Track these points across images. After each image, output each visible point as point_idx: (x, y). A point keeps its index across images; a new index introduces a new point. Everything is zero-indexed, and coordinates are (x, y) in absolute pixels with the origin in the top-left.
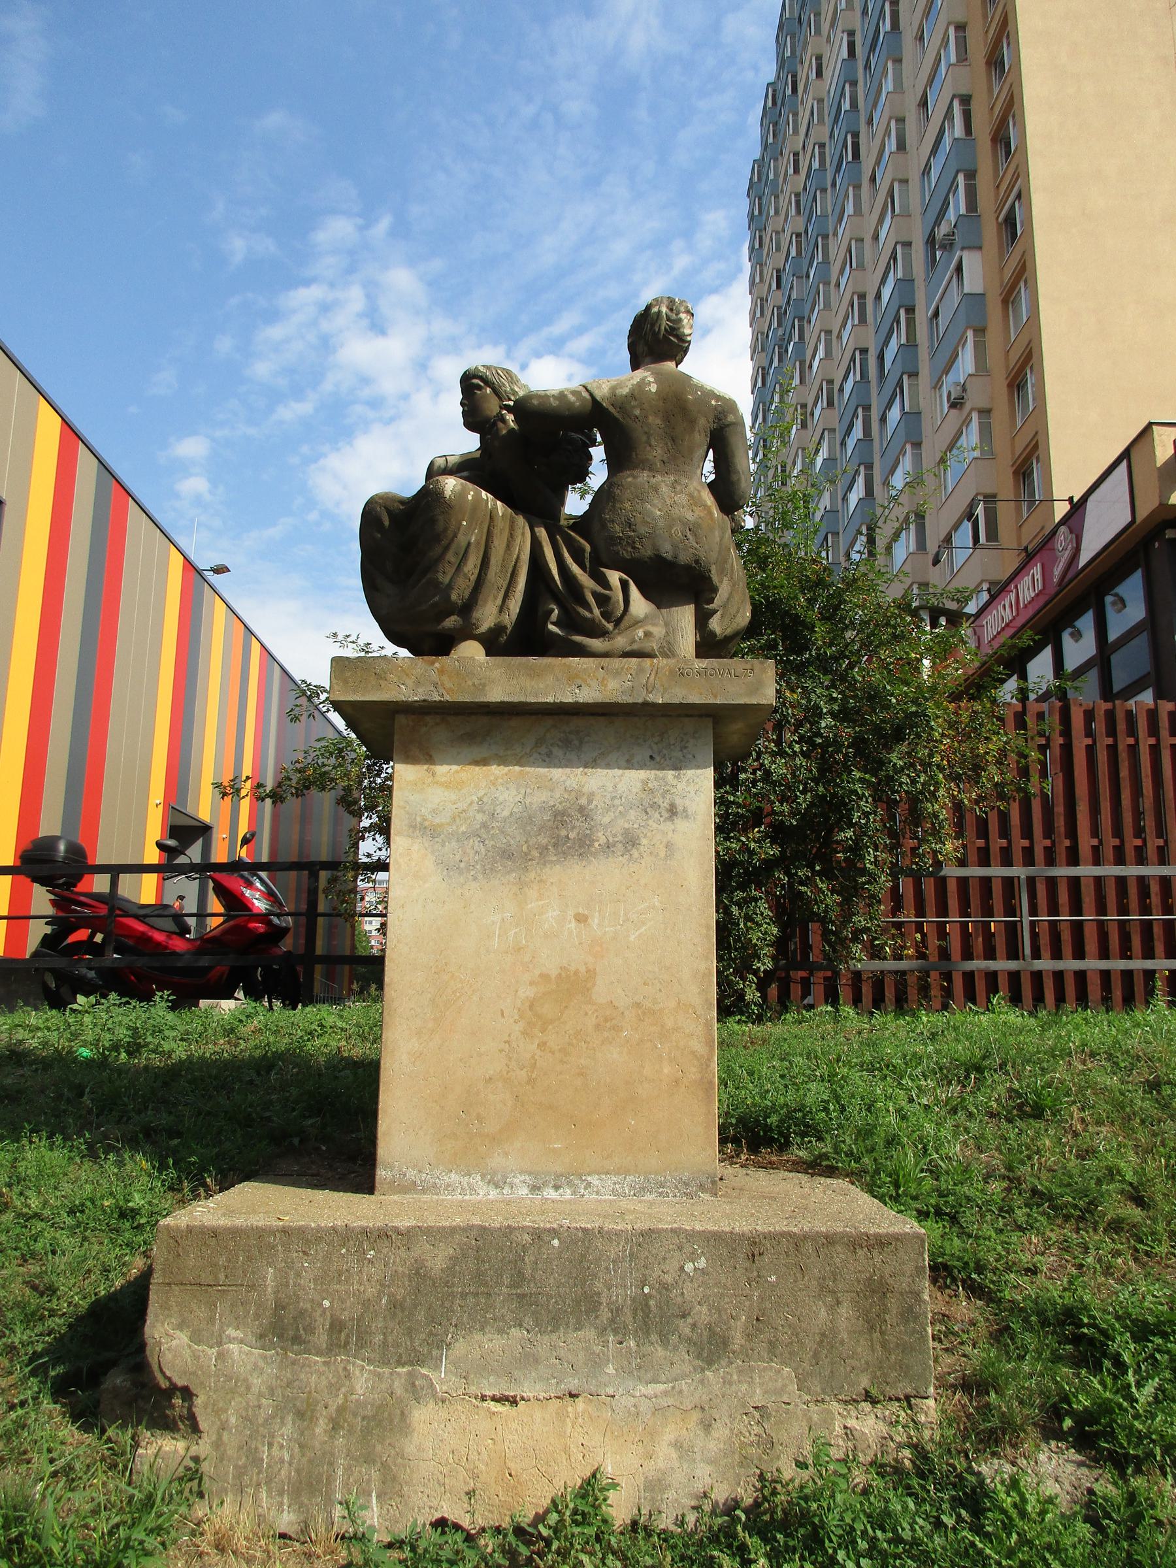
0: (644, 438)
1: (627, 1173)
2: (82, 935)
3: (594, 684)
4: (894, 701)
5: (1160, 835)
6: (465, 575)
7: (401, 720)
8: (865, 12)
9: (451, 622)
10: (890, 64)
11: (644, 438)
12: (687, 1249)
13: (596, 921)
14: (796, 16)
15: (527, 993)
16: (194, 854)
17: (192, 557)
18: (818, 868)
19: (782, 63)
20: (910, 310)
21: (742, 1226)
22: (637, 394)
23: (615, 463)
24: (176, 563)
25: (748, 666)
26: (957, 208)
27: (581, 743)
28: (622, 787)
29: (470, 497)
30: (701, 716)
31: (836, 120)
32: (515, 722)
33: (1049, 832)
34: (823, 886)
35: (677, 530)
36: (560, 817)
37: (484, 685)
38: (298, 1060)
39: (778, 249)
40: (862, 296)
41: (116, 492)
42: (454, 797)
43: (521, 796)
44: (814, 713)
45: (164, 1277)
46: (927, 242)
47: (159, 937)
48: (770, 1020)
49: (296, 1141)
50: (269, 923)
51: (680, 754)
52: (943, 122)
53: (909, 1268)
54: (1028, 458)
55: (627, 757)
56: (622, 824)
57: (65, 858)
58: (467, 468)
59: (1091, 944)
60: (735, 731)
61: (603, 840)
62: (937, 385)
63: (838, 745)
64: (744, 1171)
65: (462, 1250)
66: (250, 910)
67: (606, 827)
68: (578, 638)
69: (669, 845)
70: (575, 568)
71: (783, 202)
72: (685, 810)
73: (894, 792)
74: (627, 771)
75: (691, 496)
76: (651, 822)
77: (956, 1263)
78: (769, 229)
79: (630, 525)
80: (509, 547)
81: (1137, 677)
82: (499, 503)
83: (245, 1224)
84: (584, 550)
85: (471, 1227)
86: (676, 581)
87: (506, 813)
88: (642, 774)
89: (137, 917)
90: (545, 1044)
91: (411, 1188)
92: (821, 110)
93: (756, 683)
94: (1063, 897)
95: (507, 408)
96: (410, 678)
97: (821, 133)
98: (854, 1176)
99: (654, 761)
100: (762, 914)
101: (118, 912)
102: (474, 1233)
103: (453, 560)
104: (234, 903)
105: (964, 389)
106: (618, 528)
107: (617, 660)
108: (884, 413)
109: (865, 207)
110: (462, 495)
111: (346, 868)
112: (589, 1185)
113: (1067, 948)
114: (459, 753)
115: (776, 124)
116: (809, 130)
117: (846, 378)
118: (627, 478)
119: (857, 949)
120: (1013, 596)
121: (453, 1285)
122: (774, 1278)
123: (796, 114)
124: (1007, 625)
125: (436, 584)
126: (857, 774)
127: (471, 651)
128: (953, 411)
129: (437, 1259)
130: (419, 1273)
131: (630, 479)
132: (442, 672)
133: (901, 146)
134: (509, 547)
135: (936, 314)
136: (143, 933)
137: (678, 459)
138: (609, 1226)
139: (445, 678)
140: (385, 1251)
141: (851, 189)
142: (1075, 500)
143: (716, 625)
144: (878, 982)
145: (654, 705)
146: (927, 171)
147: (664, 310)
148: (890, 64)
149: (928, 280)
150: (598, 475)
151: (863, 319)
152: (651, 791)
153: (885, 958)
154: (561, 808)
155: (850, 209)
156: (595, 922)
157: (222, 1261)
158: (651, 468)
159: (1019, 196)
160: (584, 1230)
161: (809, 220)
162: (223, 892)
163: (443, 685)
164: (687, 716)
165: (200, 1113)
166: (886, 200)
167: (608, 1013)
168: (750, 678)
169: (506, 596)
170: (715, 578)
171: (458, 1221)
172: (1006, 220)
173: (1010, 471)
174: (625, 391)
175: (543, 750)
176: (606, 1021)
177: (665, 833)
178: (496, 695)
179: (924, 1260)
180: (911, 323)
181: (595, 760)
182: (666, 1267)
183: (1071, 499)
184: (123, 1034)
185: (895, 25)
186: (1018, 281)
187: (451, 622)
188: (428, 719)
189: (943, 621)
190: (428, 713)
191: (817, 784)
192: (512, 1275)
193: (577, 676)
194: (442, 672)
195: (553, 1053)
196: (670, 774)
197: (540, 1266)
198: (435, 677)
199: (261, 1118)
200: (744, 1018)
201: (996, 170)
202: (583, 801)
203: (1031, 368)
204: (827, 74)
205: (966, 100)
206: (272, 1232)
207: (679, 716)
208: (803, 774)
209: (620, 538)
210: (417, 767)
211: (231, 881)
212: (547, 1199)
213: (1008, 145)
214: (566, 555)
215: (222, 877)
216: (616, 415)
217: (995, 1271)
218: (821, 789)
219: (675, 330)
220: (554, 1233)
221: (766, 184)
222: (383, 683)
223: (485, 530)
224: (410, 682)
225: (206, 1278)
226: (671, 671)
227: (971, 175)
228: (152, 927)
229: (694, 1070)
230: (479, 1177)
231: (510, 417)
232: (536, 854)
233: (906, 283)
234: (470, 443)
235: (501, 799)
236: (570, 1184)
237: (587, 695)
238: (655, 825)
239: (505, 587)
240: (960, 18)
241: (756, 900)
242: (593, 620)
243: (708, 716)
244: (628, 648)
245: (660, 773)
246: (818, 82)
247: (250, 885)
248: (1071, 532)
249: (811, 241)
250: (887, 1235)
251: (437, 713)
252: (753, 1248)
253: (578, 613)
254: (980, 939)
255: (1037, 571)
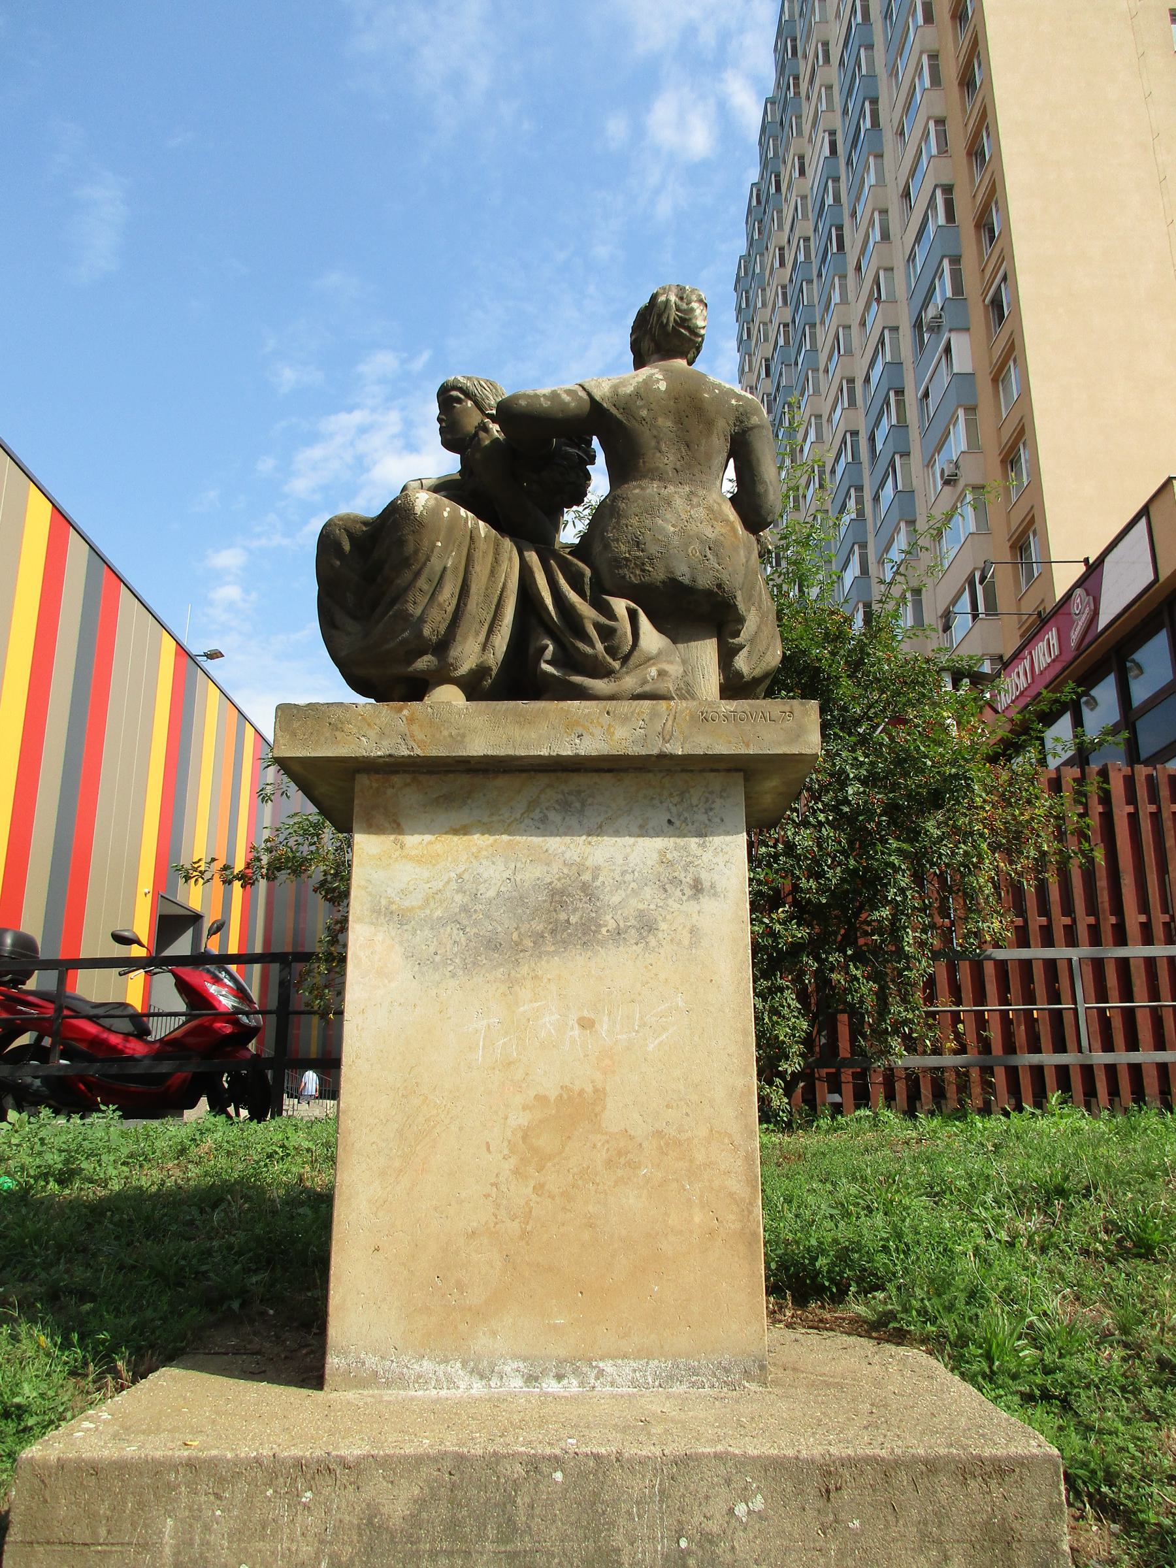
0: (653, 443)
1: (650, 1356)
2: (25, 1039)
3: (597, 731)
4: (929, 763)
5: (1165, 910)
6: (440, 605)
7: (363, 781)
8: (845, 112)
9: (425, 662)
10: (871, 159)
11: (653, 443)
12: (738, 1485)
13: (605, 1027)
14: (778, 119)
15: (522, 1119)
16: (182, 946)
17: (185, 642)
18: (849, 952)
19: (765, 164)
20: (900, 392)
21: (811, 1447)
22: (643, 393)
23: (619, 473)
24: (168, 647)
25: (787, 708)
26: (943, 291)
27: (583, 805)
28: (634, 859)
29: (445, 514)
30: (729, 770)
31: (820, 215)
32: (501, 781)
33: (1092, 908)
34: (858, 973)
35: (695, 548)
36: (558, 897)
37: (463, 736)
38: (251, 1192)
39: (766, 340)
40: (851, 381)
41: (107, 576)
42: (426, 874)
43: (510, 872)
44: (841, 780)
45: (24, 1532)
46: (914, 326)
47: (115, 1039)
48: (800, 1127)
49: (235, 1305)
50: (236, 1023)
51: (704, 818)
52: (926, 212)
53: (1040, 1506)
54: (1025, 532)
55: (640, 822)
56: (634, 903)
57: (12, 952)
58: (444, 487)
59: (1145, 1032)
60: (771, 785)
61: (612, 925)
62: (930, 463)
63: (870, 814)
64: (790, 1334)
65: (431, 1488)
66: (214, 1008)
67: (615, 908)
68: (577, 679)
69: (693, 931)
70: (573, 596)
71: (770, 294)
72: (713, 886)
73: (932, 864)
74: (640, 840)
75: (710, 509)
76: (670, 902)
77: (1080, 1472)
78: (757, 321)
79: (638, 544)
80: (493, 573)
81: (1164, 745)
82: (481, 523)
83: (136, 1455)
84: (582, 575)
85: (444, 1455)
86: (698, 610)
87: (491, 893)
88: (659, 843)
89: (92, 1018)
90: (542, 1186)
91: (371, 1380)
92: (805, 207)
93: (793, 730)
94: (1112, 980)
95: (489, 416)
96: (376, 730)
97: (806, 227)
98: (935, 1344)
99: (672, 827)
100: (789, 1006)
101: (66, 1012)
102: (448, 1464)
103: (425, 587)
104: (196, 998)
105: (957, 467)
106: (623, 548)
107: (627, 703)
108: (877, 492)
109: (851, 296)
110: (436, 511)
111: (319, 959)
112: (601, 1373)
113: (1119, 1038)
114: (432, 821)
115: (760, 222)
116: (794, 224)
117: (837, 459)
118: (634, 490)
119: (896, 1043)
120: (1027, 663)
121: (419, 1540)
122: (857, 1523)
123: (780, 212)
124: (1022, 693)
125: (405, 617)
126: (895, 844)
127: (449, 696)
128: (947, 488)
129: (397, 1504)
130: (372, 1524)
131: (637, 491)
132: (411, 720)
133: (886, 236)
134: (493, 573)
135: (926, 395)
136: (97, 1037)
137: (693, 468)
138: (631, 1451)
139: (415, 728)
140: (326, 1491)
141: (836, 279)
142: (1091, 561)
143: (742, 663)
144: (913, 1080)
145: (672, 757)
146: (912, 258)
147: (673, 298)
148: (871, 159)
149: (917, 363)
150: (599, 485)
151: (852, 402)
152: (670, 863)
153: (924, 1053)
154: (559, 885)
155: (836, 298)
156: (603, 1027)
157: (103, 1509)
158: (662, 478)
159: (1005, 279)
160: (597, 1457)
161: (796, 310)
162: (184, 987)
163: (412, 736)
164: (712, 770)
165: (121, 1268)
166: (872, 288)
167: (622, 1144)
168: (790, 723)
169: (490, 631)
170: (741, 607)
171: (425, 1444)
172: (992, 302)
173: (1008, 545)
174: (629, 389)
175: (537, 814)
176: (620, 1154)
177: (688, 915)
178: (477, 747)
179: (1060, 1494)
180: (900, 404)
181: (601, 827)
182: (708, 1511)
183: (1086, 561)
184: (54, 1159)
185: (875, 122)
186: (1007, 359)
187: (425, 662)
188: (397, 779)
189: (966, 681)
190: (396, 772)
191: (847, 858)
192: (500, 1525)
193: (577, 723)
194: (411, 720)
195: (553, 1198)
196: (693, 842)
197: (537, 1511)
198: (402, 726)
199: (197, 1273)
200: (771, 1126)
201: (980, 254)
202: (586, 877)
203: (1024, 444)
204: (810, 172)
205: (948, 189)
206: (174, 1466)
207: (702, 771)
208: (831, 846)
209: (626, 559)
210: (382, 838)
211: (190, 974)
212: (546, 1393)
213: (992, 231)
214: (562, 582)
215: (186, 972)
216: (619, 416)
217: (1130, 1478)
218: (852, 862)
219: (685, 321)
220: (556, 1462)
221: (753, 278)
222: (337, 733)
223: (465, 553)
224: (372, 734)
225: (81, 1533)
226: (692, 716)
227: (956, 260)
228: (109, 1030)
229: (732, 1217)
230: (459, 1365)
231: (495, 428)
232: (528, 943)
233: (896, 366)
234: (449, 464)
235: (485, 875)
236: (576, 1372)
237: (590, 746)
238: (676, 906)
239: (489, 619)
240: (938, 112)
241: (781, 990)
242: (595, 657)
243: (737, 770)
244: (639, 690)
245: (681, 841)
246: (802, 180)
247: (217, 981)
248: (1088, 595)
249: (797, 332)
250: (1009, 1457)
251: (405, 772)
252: (826, 1481)
253: (578, 649)
254: (1023, 1027)
255: (1052, 636)
